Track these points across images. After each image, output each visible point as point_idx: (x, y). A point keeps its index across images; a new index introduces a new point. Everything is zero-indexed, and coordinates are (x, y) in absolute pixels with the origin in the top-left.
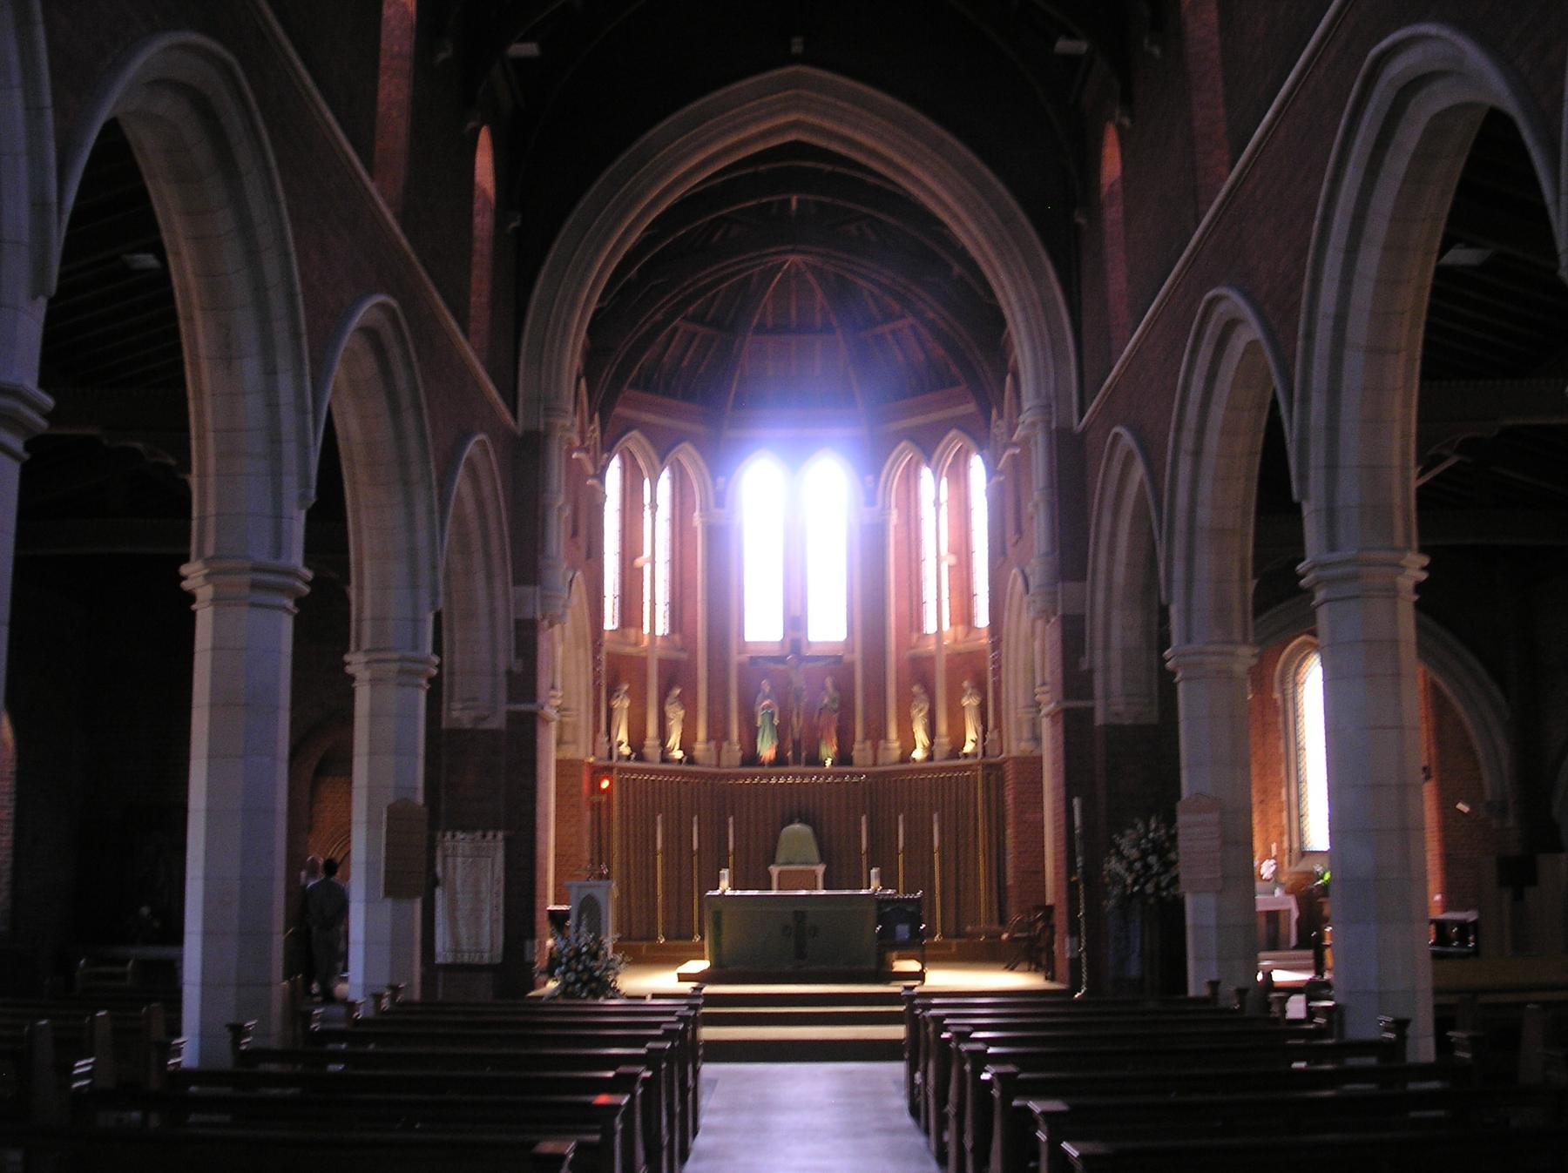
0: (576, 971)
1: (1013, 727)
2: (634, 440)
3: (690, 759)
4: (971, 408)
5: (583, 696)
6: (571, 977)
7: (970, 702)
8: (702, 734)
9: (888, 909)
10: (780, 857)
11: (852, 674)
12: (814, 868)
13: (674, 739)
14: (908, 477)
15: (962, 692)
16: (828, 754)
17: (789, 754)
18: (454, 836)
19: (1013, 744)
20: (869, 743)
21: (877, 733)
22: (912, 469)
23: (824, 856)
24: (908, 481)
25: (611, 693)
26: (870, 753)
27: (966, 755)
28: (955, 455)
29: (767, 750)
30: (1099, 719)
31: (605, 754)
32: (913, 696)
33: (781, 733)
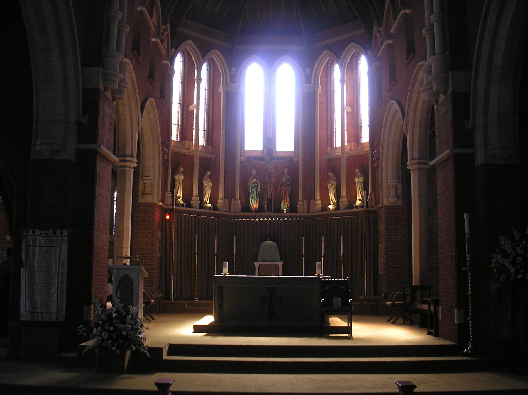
0: (108, 331)
1: (385, 191)
2: (189, 45)
3: (215, 207)
4: (362, 31)
5: (157, 171)
6: (105, 335)
7: (359, 180)
8: (221, 195)
9: (328, 288)
10: (259, 259)
11: (297, 168)
12: (278, 263)
13: (207, 197)
14: (327, 71)
15: (355, 175)
16: (285, 206)
17: (265, 206)
18: (34, 232)
19: (385, 199)
20: (305, 201)
21: (310, 196)
22: (329, 66)
23: (283, 258)
24: (327, 73)
25: (174, 172)
26: (306, 206)
27: (357, 207)
28: (351, 58)
29: (254, 204)
30: (480, 160)
31: (170, 203)
32: (328, 178)
33: (261, 196)
